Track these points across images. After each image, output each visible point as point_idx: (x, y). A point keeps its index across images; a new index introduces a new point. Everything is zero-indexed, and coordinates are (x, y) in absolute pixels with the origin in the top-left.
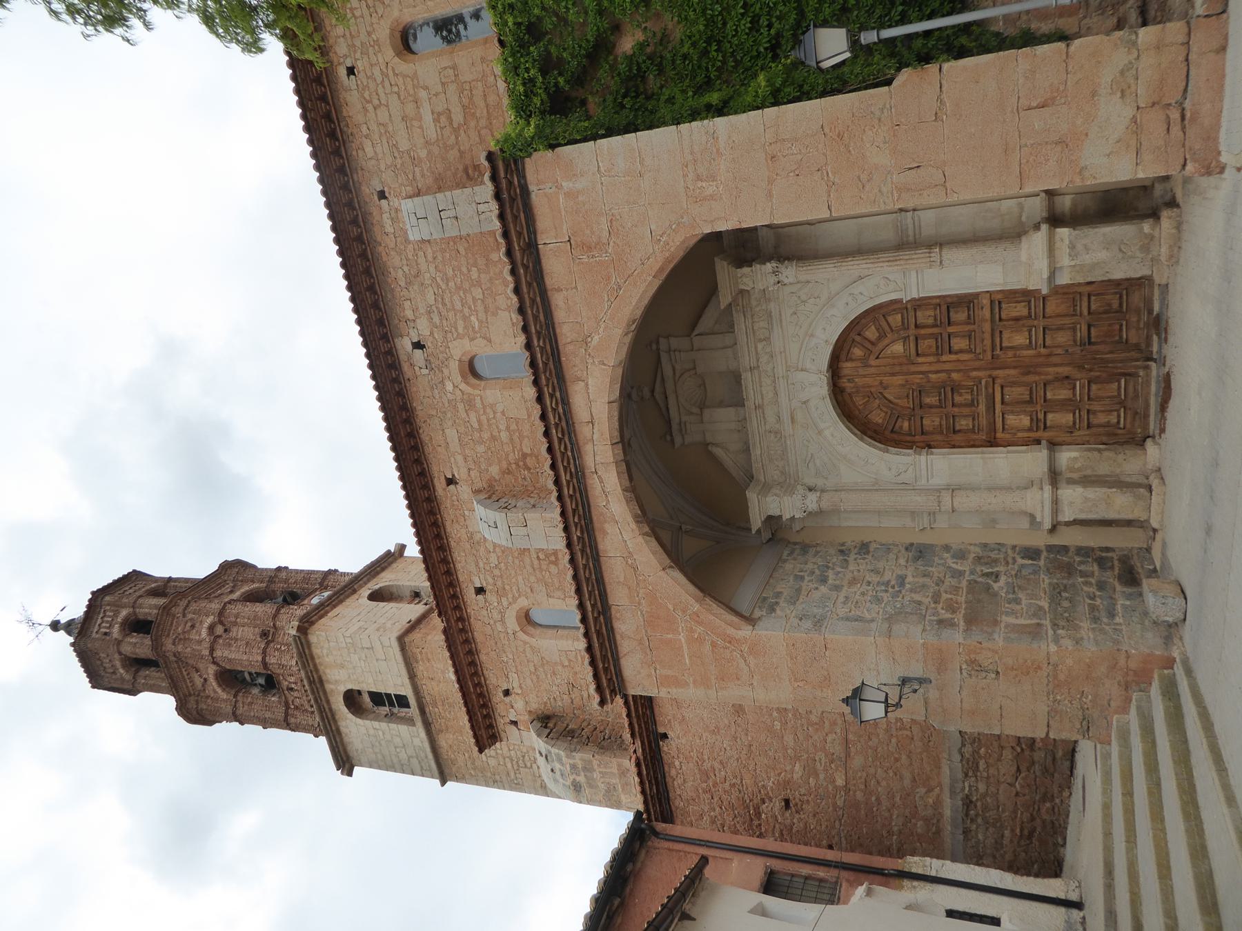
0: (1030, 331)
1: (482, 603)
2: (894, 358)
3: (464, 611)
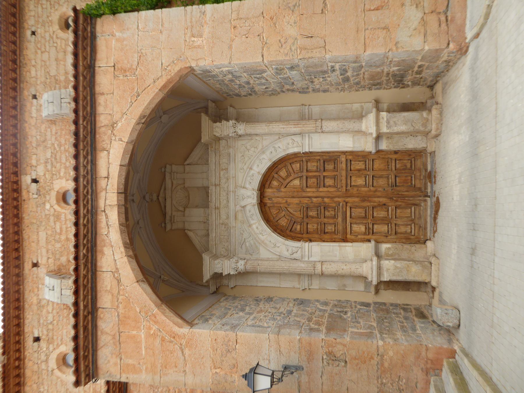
0: (366, 177)
1: (35, 349)
2: (294, 188)
3: (22, 353)
